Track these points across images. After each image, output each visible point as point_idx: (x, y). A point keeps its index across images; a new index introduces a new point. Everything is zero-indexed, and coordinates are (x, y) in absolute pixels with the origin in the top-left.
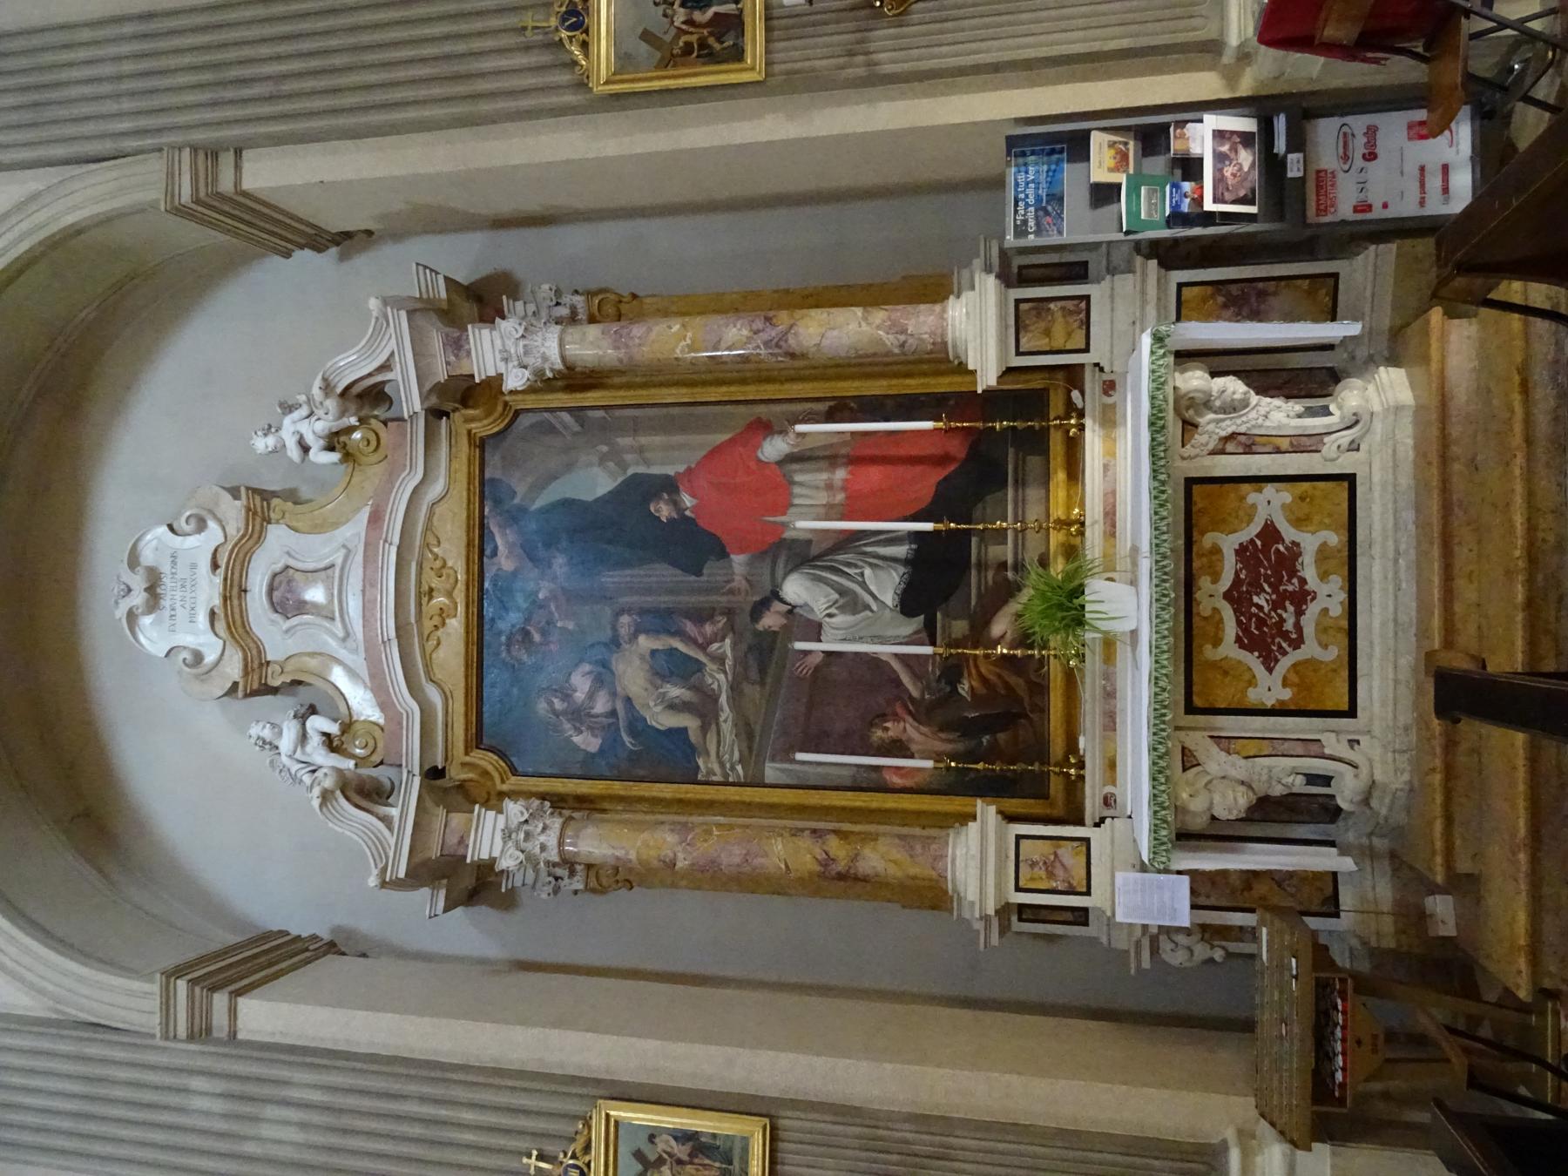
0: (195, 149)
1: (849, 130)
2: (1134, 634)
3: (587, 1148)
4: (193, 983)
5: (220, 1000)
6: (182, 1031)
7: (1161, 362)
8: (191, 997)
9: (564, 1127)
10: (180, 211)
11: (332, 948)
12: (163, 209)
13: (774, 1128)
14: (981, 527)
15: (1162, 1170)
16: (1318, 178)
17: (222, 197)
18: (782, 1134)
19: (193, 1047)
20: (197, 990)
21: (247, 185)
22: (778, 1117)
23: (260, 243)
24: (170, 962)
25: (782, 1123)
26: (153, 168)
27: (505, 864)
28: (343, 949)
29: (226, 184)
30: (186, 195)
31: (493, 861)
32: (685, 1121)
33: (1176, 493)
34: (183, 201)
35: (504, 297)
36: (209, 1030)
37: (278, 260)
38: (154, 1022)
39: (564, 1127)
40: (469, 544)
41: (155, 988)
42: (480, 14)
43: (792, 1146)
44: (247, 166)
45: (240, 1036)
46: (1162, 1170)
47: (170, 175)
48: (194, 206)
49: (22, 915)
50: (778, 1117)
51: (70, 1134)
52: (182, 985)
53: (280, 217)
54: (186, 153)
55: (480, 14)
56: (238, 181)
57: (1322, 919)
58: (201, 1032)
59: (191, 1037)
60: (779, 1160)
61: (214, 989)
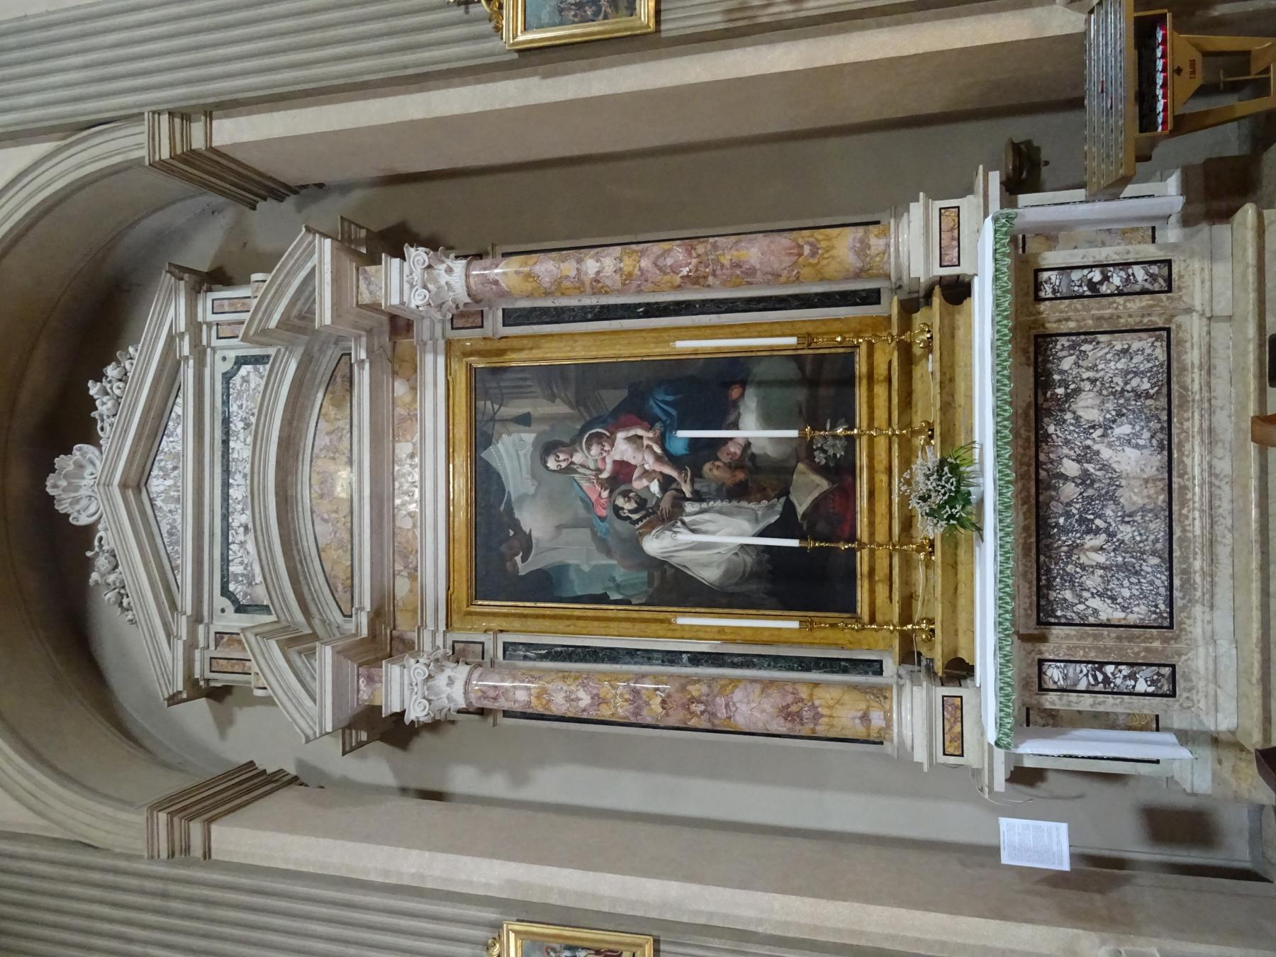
0: (171, 114)
1: (37, 145)
5: (196, 828)
6: (164, 855)
8: (170, 824)
10: (161, 166)
11: (295, 780)
12: (147, 163)
16: (869, 663)
20: (176, 820)
21: (217, 142)
24: (155, 797)
28: (305, 782)
29: (198, 143)
30: (165, 154)
32: (897, 514)
34: (163, 158)
35: (383, 255)
36: (187, 849)
38: (140, 846)
40: (517, 398)
45: (214, 857)
47: (152, 137)
48: (171, 161)
52: (163, 817)
53: (249, 174)
54: (165, 118)
56: (208, 135)
58: (179, 851)
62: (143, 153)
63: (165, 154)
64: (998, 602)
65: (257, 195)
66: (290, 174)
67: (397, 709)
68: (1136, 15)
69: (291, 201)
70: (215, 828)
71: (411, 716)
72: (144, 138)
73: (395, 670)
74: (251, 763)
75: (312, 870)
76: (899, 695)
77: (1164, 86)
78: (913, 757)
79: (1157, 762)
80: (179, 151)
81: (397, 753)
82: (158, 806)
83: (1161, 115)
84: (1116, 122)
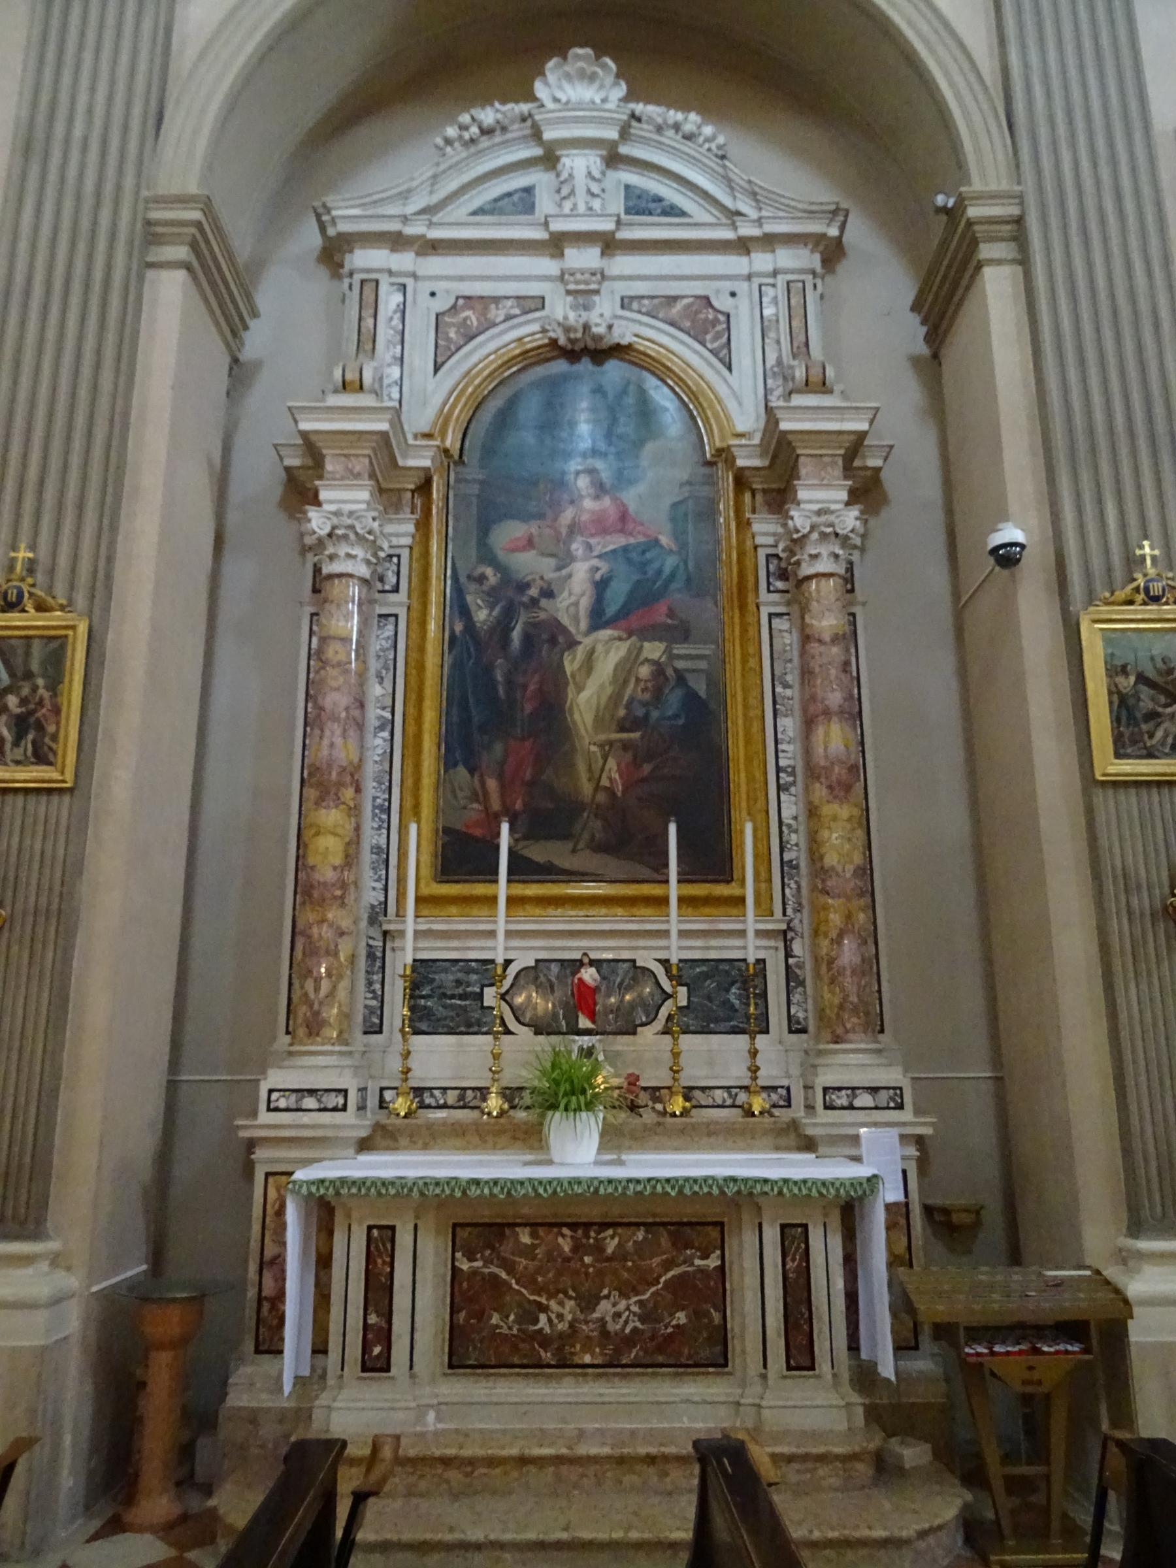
2: (550, 1162)
3: (41, 607)
4: (198, 225)
5: (181, 252)
6: (155, 215)
7: (814, 1190)
9: (60, 589)
13: (61, 791)
14: (563, 1023)
15: (1172, 803)
17: (974, 244)
18: (55, 799)
19: (139, 226)
21: (987, 271)
22: (72, 795)
23: (930, 274)
25: (66, 799)
26: (998, 181)
27: (313, 513)
29: (986, 251)
30: (973, 212)
31: (317, 503)
33: (712, 1213)
37: (910, 296)
39: (60, 589)
41: (193, 188)
42: (1162, 506)
43: (42, 809)
44: (1006, 270)
46: (1172, 803)
47: (994, 196)
49: (262, 59)
50: (72, 795)
51: (98, 352)
52: (196, 215)
54: (1014, 211)
55: (1162, 506)
56: (991, 262)
57: (190, 782)
58: (152, 234)
59: (148, 223)
60: (29, 797)
61: (194, 246)
62: (977, 185)
63: (973, 212)
64: (421, 1183)
65: (930, 309)
66: (952, 354)
67: (323, 495)
68: (1092, 1323)
69: (923, 349)
70: (181, 275)
71: (313, 513)
72: (993, 187)
73: (365, 495)
74: (255, 314)
75: (130, 444)
76: (341, 1053)
77: (1067, 1352)
78: (272, 1067)
79: (904, 1172)
80: (977, 228)
81: (316, 254)
82: (207, 206)
83: (972, 1351)
84: (995, 1302)
